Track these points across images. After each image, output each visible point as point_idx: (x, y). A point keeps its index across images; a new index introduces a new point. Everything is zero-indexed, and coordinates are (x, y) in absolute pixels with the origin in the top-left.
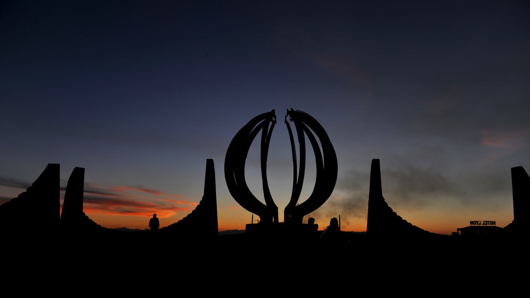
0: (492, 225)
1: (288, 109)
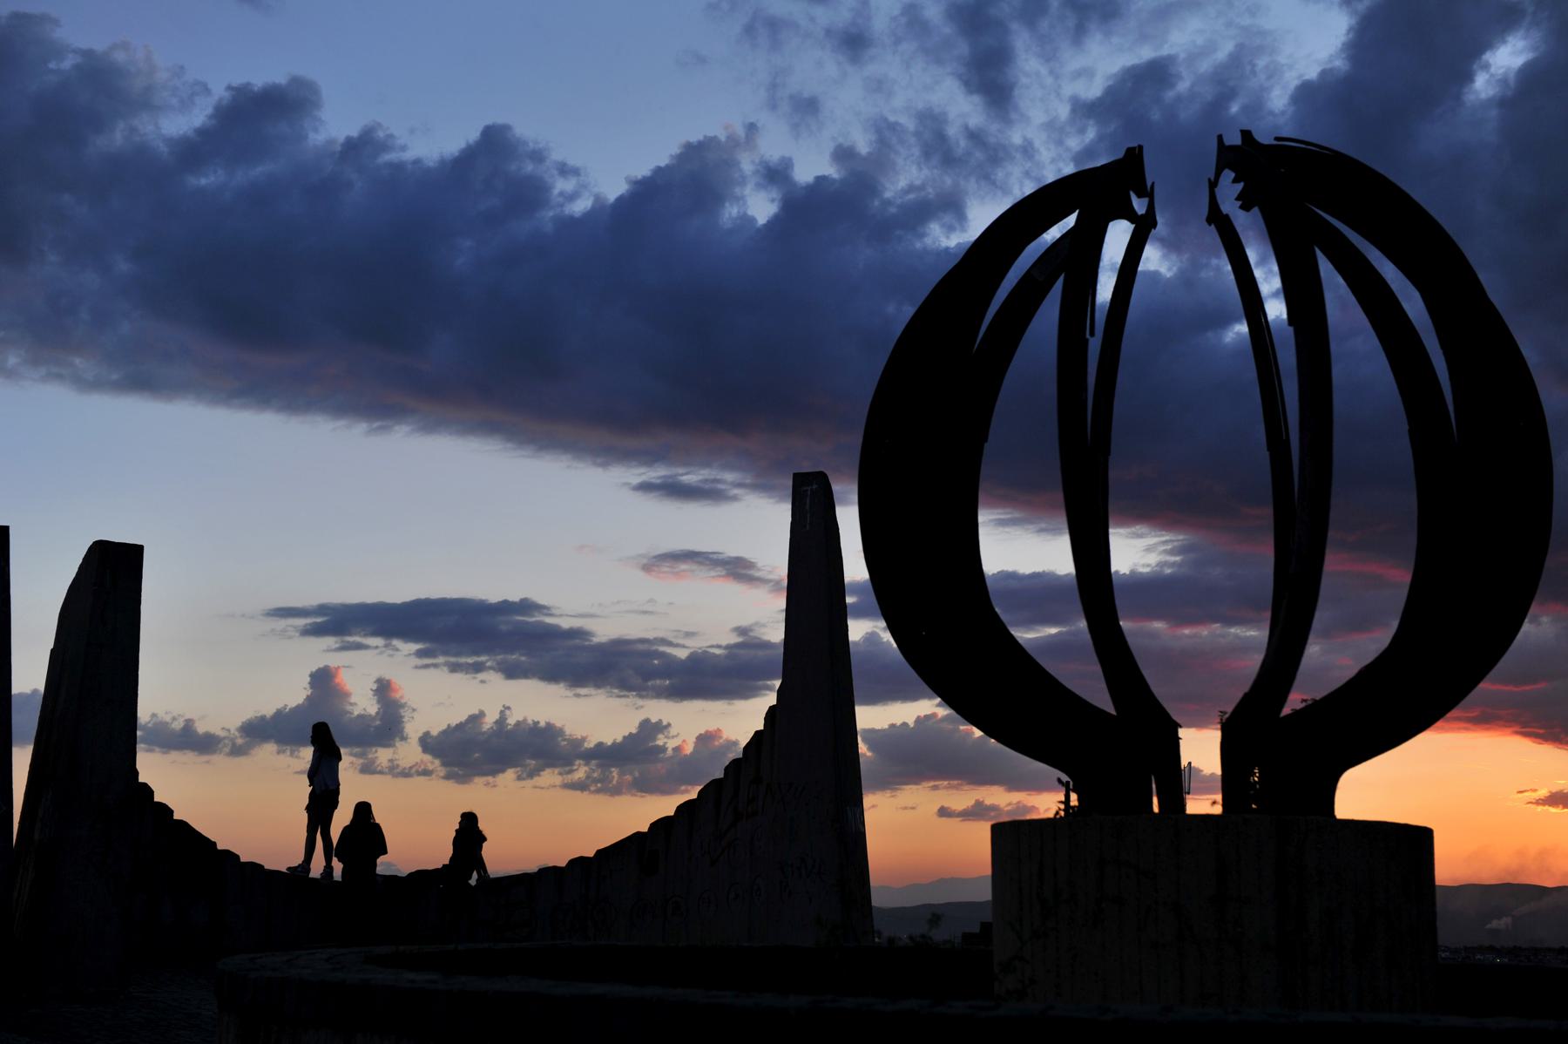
0: (937, 783)
1: (1220, 138)
